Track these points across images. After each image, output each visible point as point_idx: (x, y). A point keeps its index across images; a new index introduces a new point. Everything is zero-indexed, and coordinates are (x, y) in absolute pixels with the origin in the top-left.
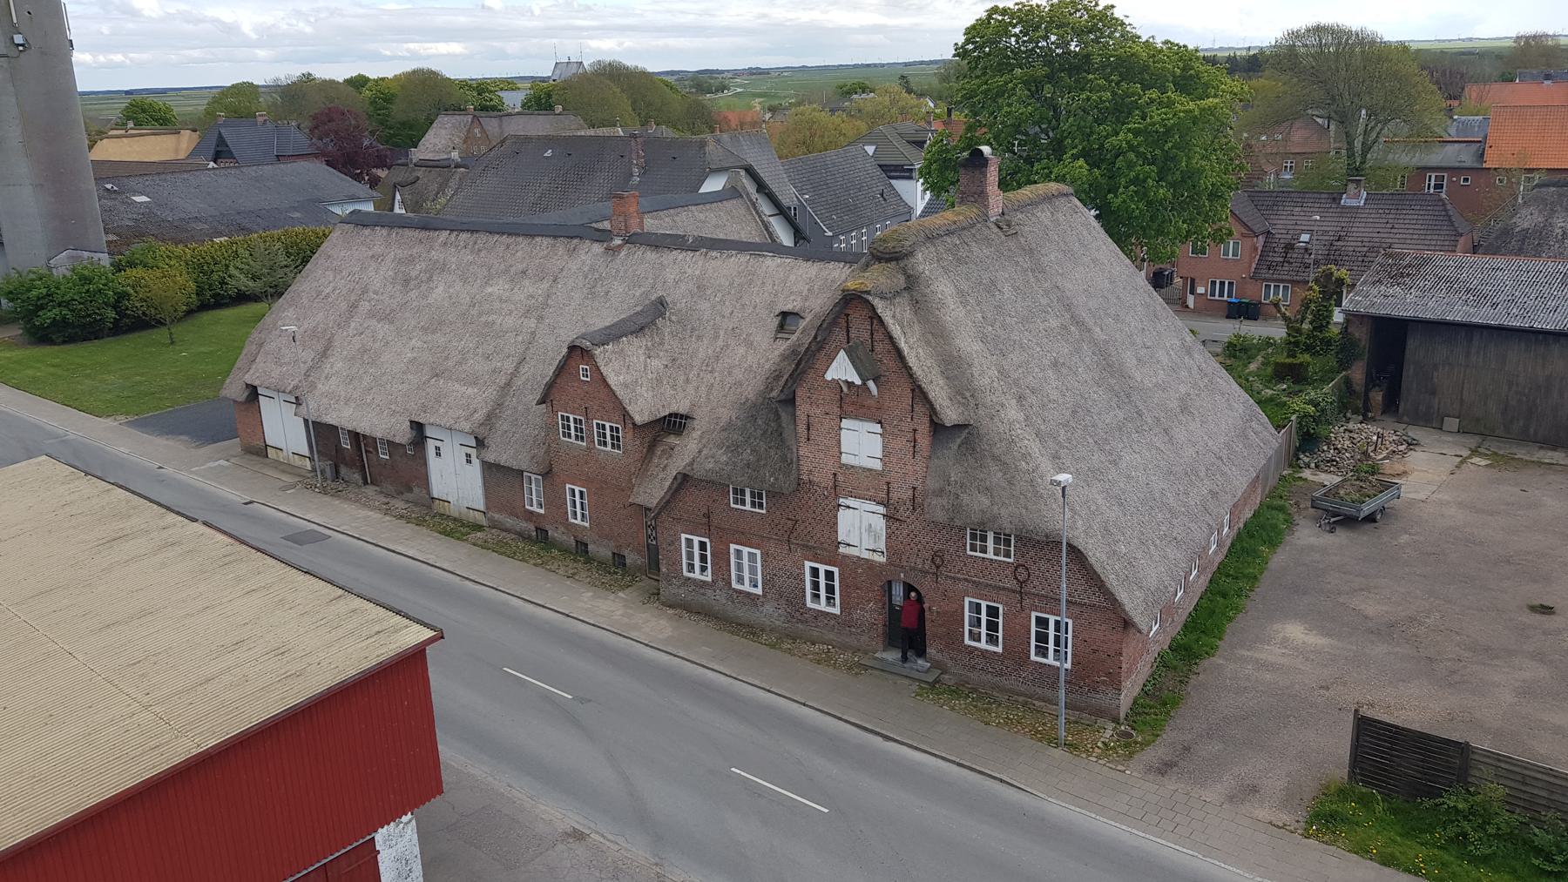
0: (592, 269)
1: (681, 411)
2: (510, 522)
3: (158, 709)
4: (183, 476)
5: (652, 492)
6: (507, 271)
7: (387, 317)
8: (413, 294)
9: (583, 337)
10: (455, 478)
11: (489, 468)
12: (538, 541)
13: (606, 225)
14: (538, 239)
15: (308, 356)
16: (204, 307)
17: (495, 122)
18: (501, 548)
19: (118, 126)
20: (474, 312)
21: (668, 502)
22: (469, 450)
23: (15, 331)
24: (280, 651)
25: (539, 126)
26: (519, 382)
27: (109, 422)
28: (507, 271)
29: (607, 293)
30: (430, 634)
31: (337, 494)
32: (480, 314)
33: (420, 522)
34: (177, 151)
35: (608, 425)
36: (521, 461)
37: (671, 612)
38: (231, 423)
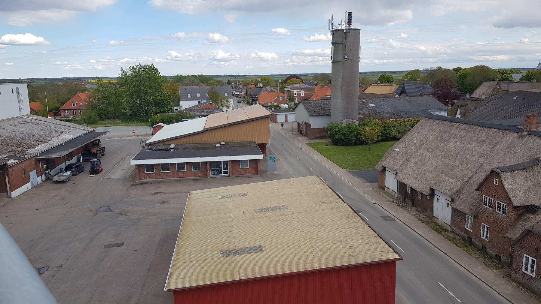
0: (511, 143)
1: (536, 205)
2: (459, 232)
3: (314, 253)
4: (359, 191)
5: (515, 234)
6: (477, 140)
7: (431, 151)
8: (442, 144)
9: (498, 168)
10: (442, 211)
11: (454, 210)
12: (468, 242)
13: (522, 127)
14: (492, 129)
15: (403, 160)
16: (383, 140)
17: (506, 85)
18: (453, 240)
19: (377, 82)
20: (462, 153)
21: (520, 240)
22: (449, 202)
23: (329, 140)
24: (351, 247)
25: (525, 87)
26: (472, 181)
27: (344, 170)
28: (477, 140)
29: (515, 153)
30: (398, 257)
31: (402, 207)
32: (463, 154)
33: (427, 223)
34: (391, 91)
35: (502, 204)
36: (466, 210)
37: (514, 284)
38: (377, 178)
